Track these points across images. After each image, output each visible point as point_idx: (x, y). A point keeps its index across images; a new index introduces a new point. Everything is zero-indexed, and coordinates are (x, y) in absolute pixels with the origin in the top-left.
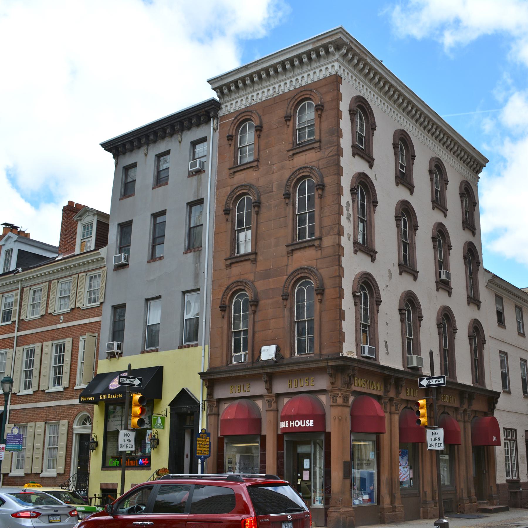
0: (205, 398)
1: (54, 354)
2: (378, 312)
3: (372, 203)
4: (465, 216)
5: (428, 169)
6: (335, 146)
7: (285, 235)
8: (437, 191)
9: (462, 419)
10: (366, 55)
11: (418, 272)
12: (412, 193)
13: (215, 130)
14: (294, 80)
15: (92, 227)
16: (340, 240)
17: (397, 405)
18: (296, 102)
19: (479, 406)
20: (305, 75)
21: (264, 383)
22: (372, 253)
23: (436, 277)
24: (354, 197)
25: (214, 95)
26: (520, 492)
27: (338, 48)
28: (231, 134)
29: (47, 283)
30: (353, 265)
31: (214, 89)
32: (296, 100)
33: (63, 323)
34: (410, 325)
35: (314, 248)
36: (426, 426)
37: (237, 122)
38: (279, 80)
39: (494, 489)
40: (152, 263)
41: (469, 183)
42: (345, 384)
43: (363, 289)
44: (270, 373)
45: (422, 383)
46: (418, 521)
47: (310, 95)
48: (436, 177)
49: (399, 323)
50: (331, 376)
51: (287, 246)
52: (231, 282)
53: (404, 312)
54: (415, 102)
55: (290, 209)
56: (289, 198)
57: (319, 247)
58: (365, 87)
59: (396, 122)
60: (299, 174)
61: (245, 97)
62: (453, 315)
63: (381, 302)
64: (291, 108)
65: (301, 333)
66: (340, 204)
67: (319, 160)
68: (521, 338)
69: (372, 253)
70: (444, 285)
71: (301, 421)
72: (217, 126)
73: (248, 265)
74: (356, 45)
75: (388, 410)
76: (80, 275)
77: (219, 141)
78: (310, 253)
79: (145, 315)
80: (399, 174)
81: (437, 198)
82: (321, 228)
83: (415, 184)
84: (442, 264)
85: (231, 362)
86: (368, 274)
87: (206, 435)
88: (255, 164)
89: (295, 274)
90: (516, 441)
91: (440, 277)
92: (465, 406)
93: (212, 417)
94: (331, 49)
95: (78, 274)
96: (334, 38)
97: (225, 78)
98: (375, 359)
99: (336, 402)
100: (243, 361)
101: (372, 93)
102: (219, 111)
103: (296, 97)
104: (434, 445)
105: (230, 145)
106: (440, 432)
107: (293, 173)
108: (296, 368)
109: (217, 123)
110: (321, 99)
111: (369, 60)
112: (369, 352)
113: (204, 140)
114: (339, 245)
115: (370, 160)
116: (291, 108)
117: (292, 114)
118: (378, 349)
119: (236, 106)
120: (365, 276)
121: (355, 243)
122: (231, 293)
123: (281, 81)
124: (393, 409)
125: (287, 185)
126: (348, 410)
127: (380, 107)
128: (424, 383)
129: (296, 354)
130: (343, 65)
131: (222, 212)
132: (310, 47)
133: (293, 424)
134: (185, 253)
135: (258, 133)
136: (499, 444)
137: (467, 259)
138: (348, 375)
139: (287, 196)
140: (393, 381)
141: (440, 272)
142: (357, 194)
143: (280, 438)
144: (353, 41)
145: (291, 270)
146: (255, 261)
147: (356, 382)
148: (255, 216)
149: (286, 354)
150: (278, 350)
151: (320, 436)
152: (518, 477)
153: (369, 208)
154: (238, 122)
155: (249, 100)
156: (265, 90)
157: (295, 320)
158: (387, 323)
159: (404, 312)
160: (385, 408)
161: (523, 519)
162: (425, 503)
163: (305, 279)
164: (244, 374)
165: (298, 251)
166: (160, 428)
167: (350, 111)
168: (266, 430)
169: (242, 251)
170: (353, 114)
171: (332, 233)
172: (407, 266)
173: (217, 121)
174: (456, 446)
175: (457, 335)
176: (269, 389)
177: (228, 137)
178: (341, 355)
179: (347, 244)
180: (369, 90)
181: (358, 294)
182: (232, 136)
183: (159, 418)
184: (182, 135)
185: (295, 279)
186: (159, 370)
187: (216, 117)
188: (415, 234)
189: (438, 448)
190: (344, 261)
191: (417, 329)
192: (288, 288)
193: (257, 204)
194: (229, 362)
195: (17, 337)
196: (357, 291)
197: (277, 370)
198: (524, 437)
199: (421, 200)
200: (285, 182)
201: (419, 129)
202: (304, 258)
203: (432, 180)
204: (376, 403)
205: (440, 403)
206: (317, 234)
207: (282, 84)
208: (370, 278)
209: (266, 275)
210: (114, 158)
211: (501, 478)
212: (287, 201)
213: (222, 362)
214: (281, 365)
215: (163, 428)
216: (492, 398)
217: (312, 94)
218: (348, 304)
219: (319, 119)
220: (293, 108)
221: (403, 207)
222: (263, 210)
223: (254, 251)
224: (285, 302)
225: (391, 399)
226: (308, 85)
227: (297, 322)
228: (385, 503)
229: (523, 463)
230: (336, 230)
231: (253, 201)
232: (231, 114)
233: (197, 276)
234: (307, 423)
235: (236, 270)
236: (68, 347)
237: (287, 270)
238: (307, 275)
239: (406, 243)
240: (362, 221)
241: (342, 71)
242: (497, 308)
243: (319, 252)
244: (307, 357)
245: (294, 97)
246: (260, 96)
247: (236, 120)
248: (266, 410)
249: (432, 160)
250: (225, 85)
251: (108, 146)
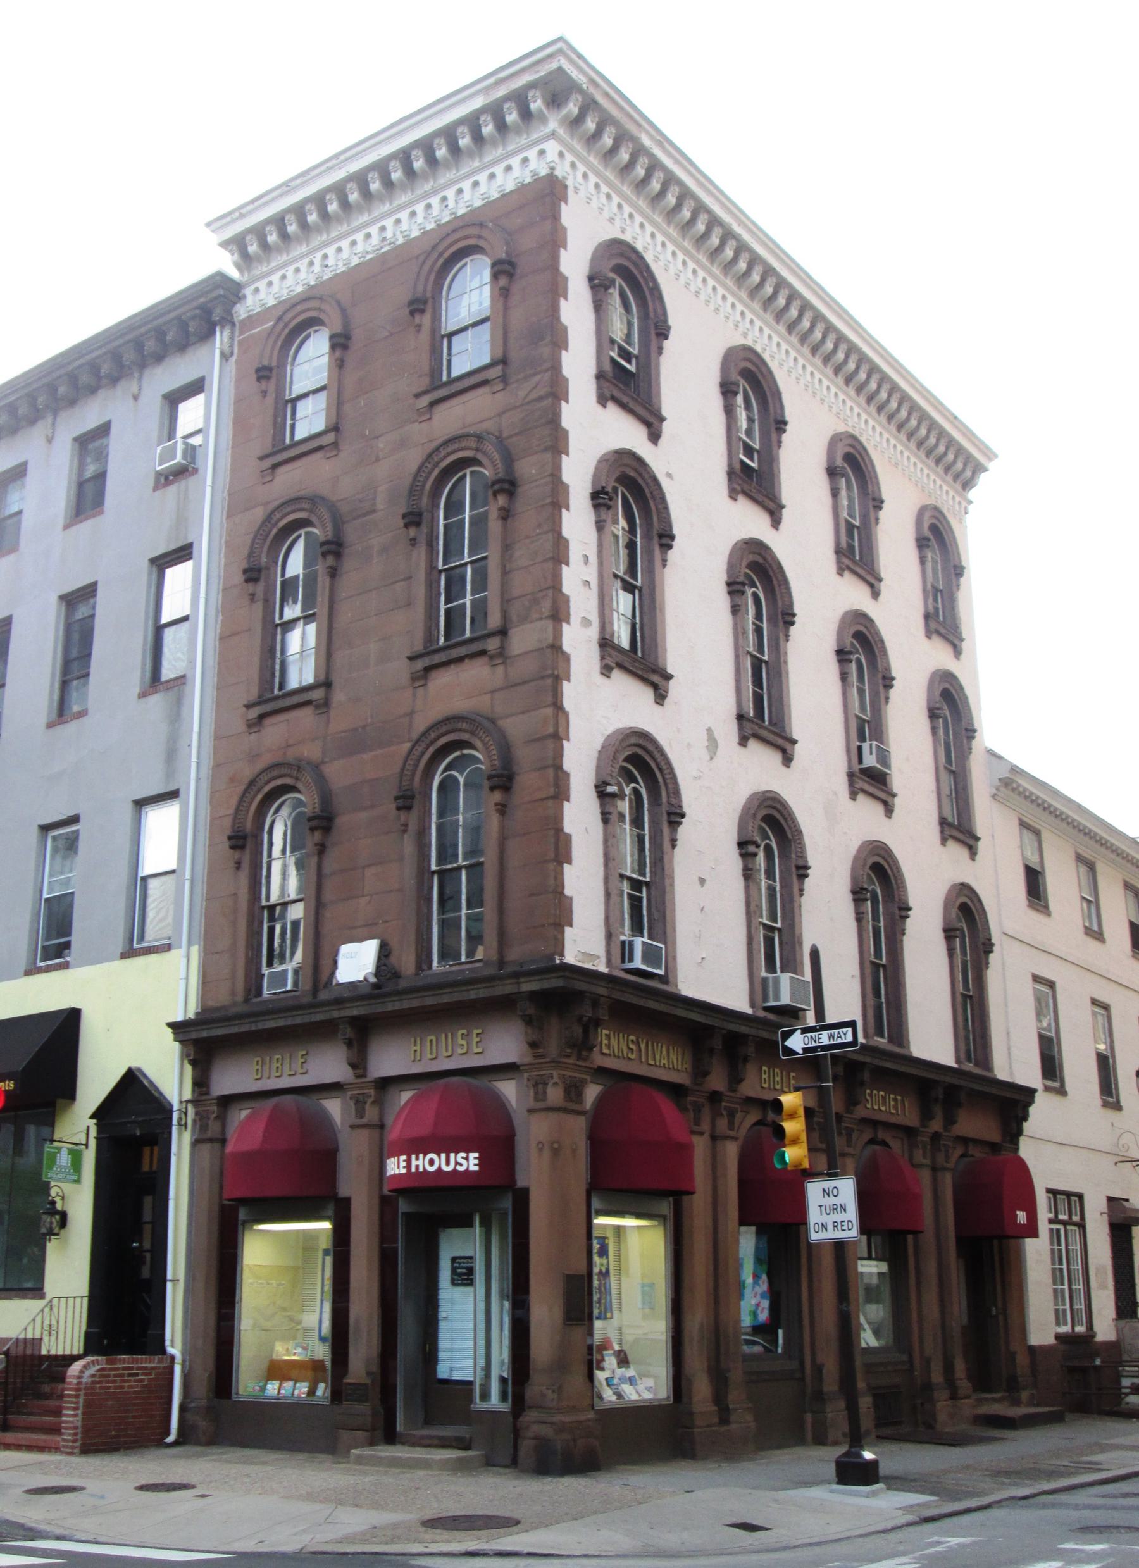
0: (188, 1095)
2: (674, 846)
3: (656, 540)
4: (930, 600)
5: (825, 465)
6: (547, 370)
7: (405, 628)
8: (850, 527)
9: (927, 1162)
10: (639, 125)
11: (795, 742)
12: (776, 522)
13: (225, 357)
14: (435, 201)
16: (558, 635)
17: (731, 1114)
18: (441, 261)
19: (975, 1124)
20: (466, 185)
21: (344, 1048)
22: (655, 678)
23: (849, 761)
24: (604, 517)
25: (226, 264)
26: (1096, 1368)
27: (555, 101)
28: (266, 363)
30: (597, 709)
31: (225, 244)
32: (441, 255)
34: (771, 890)
35: (483, 660)
36: (804, 1170)
37: (283, 330)
38: (395, 204)
39: (1022, 1360)
40: (60, 728)
41: (941, 513)
42: (573, 1045)
43: (632, 779)
44: (359, 1020)
45: (789, 1043)
46: (799, 1451)
47: (479, 237)
48: (849, 487)
49: (739, 883)
50: (528, 1021)
51: (411, 658)
52: (260, 766)
53: (752, 849)
54: (785, 273)
55: (420, 554)
56: (418, 524)
57: (502, 656)
58: (638, 219)
59: (731, 324)
60: (445, 457)
61: (306, 261)
62: (898, 868)
63: (683, 816)
64: (427, 280)
65: (448, 901)
66: (559, 533)
67: (500, 414)
68: (1093, 944)
69: (655, 678)
70: (871, 781)
71: (443, 1155)
72: (232, 346)
73: (306, 715)
74: (607, 95)
75: (706, 1126)
77: (237, 387)
78: (476, 673)
79: (37, 870)
80: (737, 466)
81: (851, 547)
82: (506, 601)
83: (785, 498)
84: (867, 728)
85: (259, 993)
86: (645, 736)
88: (330, 438)
89: (433, 735)
90: (1082, 1225)
91: (860, 761)
92: (936, 1125)
93: (206, 1147)
94: (537, 105)
96: (543, 70)
97: (250, 212)
98: (664, 979)
99: (544, 1099)
100: (289, 987)
101: (660, 238)
102: (238, 305)
103: (441, 248)
104: (830, 1227)
105: (264, 393)
106: (846, 1189)
107: (430, 456)
108: (430, 1001)
109: (232, 338)
110: (507, 243)
111: (646, 142)
112: (646, 958)
113: (196, 387)
114: (556, 647)
115: (651, 419)
116: (427, 280)
117: (429, 295)
118: (674, 949)
119: (281, 288)
120: (633, 740)
121: (606, 644)
122: (259, 797)
123: (400, 208)
124: (722, 1124)
125: (414, 491)
126: (577, 1128)
127: (682, 280)
128: (797, 1042)
129: (435, 964)
130: (572, 150)
131: (239, 578)
132: (478, 103)
133: (420, 1163)
134: (143, 695)
135: (338, 353)
136: (1034, 1234)
137: (938, 717)
138: (580, 1019)
139: (413, 519)
140: (717, 1043)
141: (860, 748)
142: (609, 508)
143: (386, 1204)
144: (597, 79)
145: (421, 724)
146: (324, 705)
147: (605, 1042)
148: (328, 580)
149: (406, 962)
150: (384, 953)
151: (493, 1198)
152: (1090, 1326)
153: (648, 552)
154: (287, 331)
155: (317, 268)
156: (359, 236)
157: (434, 867)
158: (702, 881)
159: (752, 849)
160: (697, 1122)
161: (1103, 1448)
162: (819, 1397)
163: (461, 749)
164: (289, 1022)
165: (442, 671)
166: (69, 1181)
167: (591, 279)
168: (353, 1183)
169: (293, 683)
170: (600, 285)
171: (535, 616)
172: (763, 720)
173: (232, 332)
174: (910, 1238)
175: (911, 924)
176: (359, 1065)
177: (258, 370)
178: (558, 961)
179: (579, 640)
180: (649, 229)
181: (612, 789)
182: (270, 369)
183: (64, 1152)
184: (140, 379)
185: (432, 750)
186: (70, 1019)
187: (228, 320)
188: (787, 636)
189: (839, 1235)
190: (571, 694)
191: (792, 901)
192: (413, 775)
193: (333, 547)
194: (253, 992)
196: (608, 779)
197: (379, 1009)
198: (1105, 1217)
199: (804, 544)
200: (407, 482)
201: (798, 352)
202: (461, 688)
203: (835, 493)
204: (666, 1105)
205: (860, 1112)
206: (494, 620)
207: (404, 215)
208: (651, 748)
209: (354, 743)
211: (1042, 1325)
212: (412, 532)
213: (233, 993)
214: (389, 994)
215: (78, 1181)
216: (1013, 1104)
217: (485, 233)
218: (580, 816)
219: (502, 299)
220: (433, 277)
221: (752, 557)
222: (349, 564)
223: (322, 678)
224: (403, 815)
225: (715, 1097)
226: (474, 212)
227: (439, 872)
228: (695, 1399)
229: (1103, 1286)
230: (546, 606)
231: (322, 539)
232: (268, 310)
233: (172, 754)
234: (460, 1160)
235: (275, 732)
237: (410, 725)
238: (465, 736)
239: (761, 661)
240: (629, 588)
241: (568, 168)
242: (1024, 858)
243: (500, 670)
244: (463, 971)
245: (434, 248)
246: (345, 254)
247: (281, 325)
248: (352, 1127)
249: (835, 440)
250: (258, 242)
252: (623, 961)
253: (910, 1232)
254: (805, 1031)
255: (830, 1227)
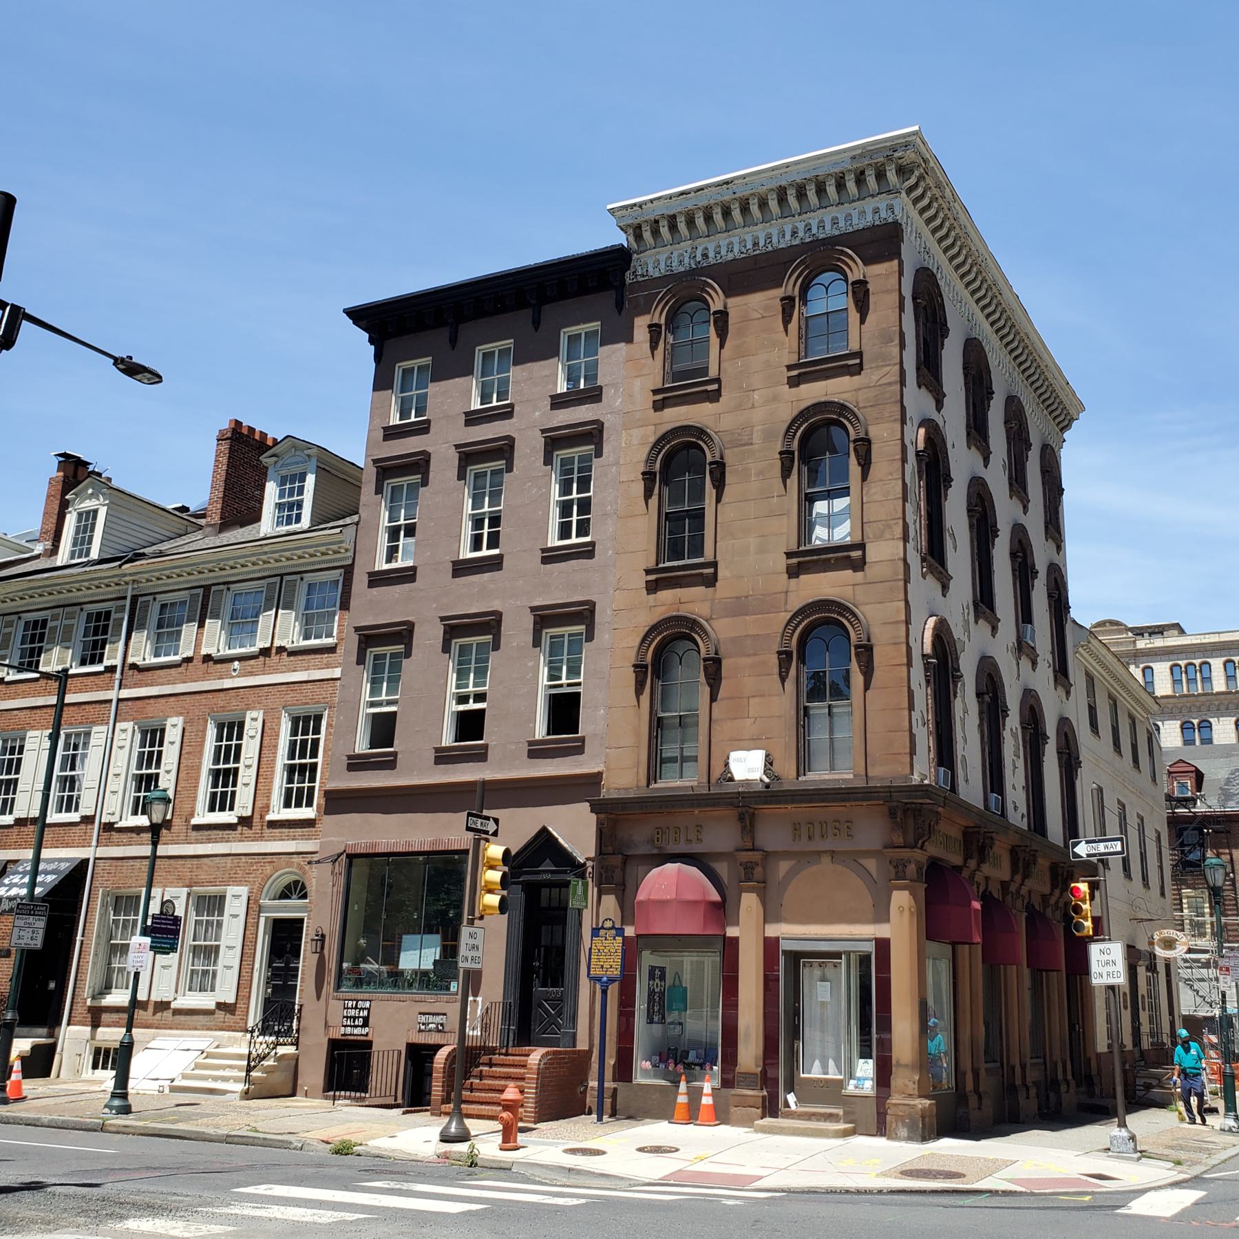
1: (137, 749)
15: (95, 518)
29: (201, 591)
33: (238, 676)
76: (286, 578)
87: (614, 932)
95: (282, 575)
104: (1105, 975)
145: (796, 603)
150: (769, 762)
189: (1111, 981)
192: (791, 637)
195: (119, 700)
209: (739, 607)
210: (371, 341)
236: (173, 735)
251: (358, 315)
252: (798, 775)
253: (1047, 971)
254: (1087, 842)
255: (1105, 975)
